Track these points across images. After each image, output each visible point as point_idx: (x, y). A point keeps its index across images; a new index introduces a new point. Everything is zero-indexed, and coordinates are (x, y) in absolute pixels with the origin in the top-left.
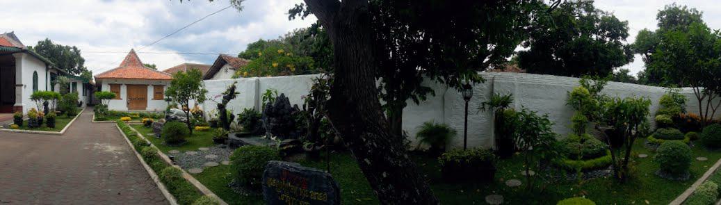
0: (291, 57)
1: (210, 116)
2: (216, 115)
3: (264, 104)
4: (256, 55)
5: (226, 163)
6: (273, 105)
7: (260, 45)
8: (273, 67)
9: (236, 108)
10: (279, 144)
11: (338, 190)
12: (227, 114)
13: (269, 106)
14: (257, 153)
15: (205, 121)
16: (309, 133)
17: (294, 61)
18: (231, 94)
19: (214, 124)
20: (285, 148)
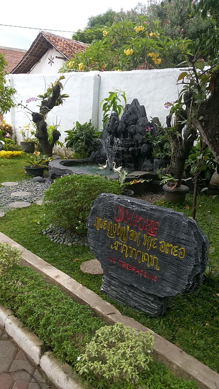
0: (156, 39)
1: (23, 134)
2: (33, 133)
3: (106, 117)
4: (100, 37)
5: (40, 203)
6: (120, 117)
7: (107, 19)
8: (125, 56)
9: (64, 120)
10: (124, 178)
11: (204, 246)
12: (48, 128)
13: (114, 120)
14: (85, 186)
15: (16, 142)
16: (174, 164)
17: (160, 45)
18: (54, 97)
19: (29, 147)
20: (132, 183)
